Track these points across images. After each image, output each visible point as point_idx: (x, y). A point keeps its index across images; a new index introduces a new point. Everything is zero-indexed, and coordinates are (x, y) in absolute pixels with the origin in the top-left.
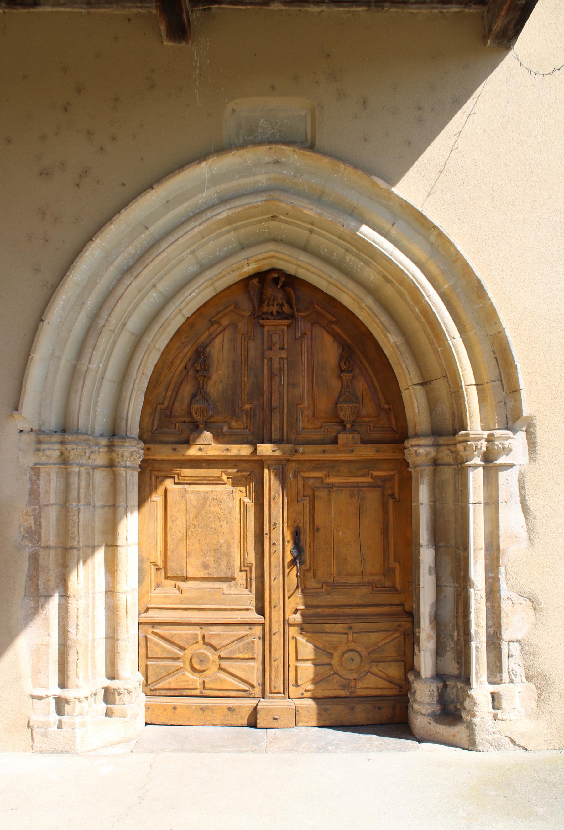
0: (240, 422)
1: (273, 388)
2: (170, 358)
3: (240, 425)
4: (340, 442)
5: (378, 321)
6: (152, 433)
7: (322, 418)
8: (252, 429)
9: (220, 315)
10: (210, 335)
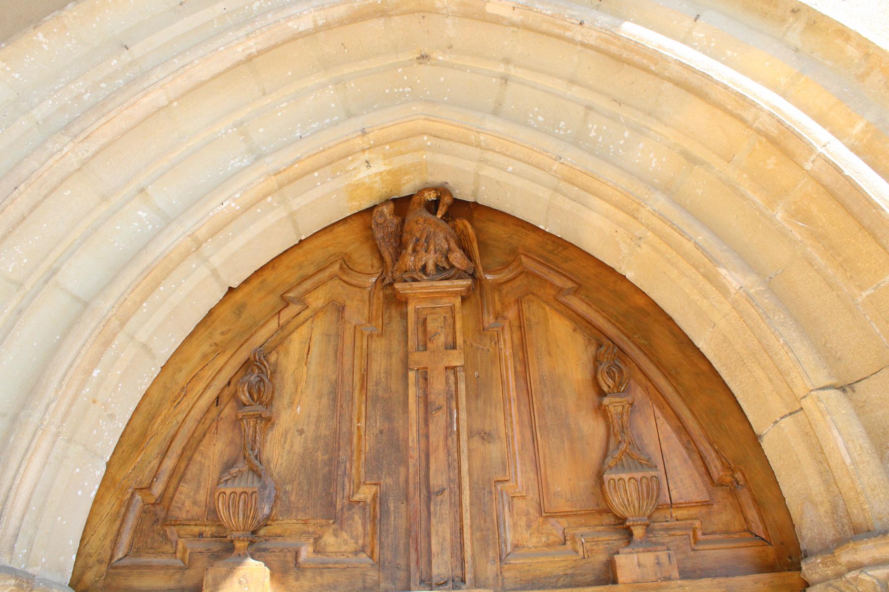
0: (345, 535)
1: (432, 439)
2: (182, 378)
3: (346, 543)
4: (623, 575)
5: (689, 246)
6: (110, 566)
7: (565, 515)
8: (377, 550)
9: (307, 285)
10: (281, 327)
